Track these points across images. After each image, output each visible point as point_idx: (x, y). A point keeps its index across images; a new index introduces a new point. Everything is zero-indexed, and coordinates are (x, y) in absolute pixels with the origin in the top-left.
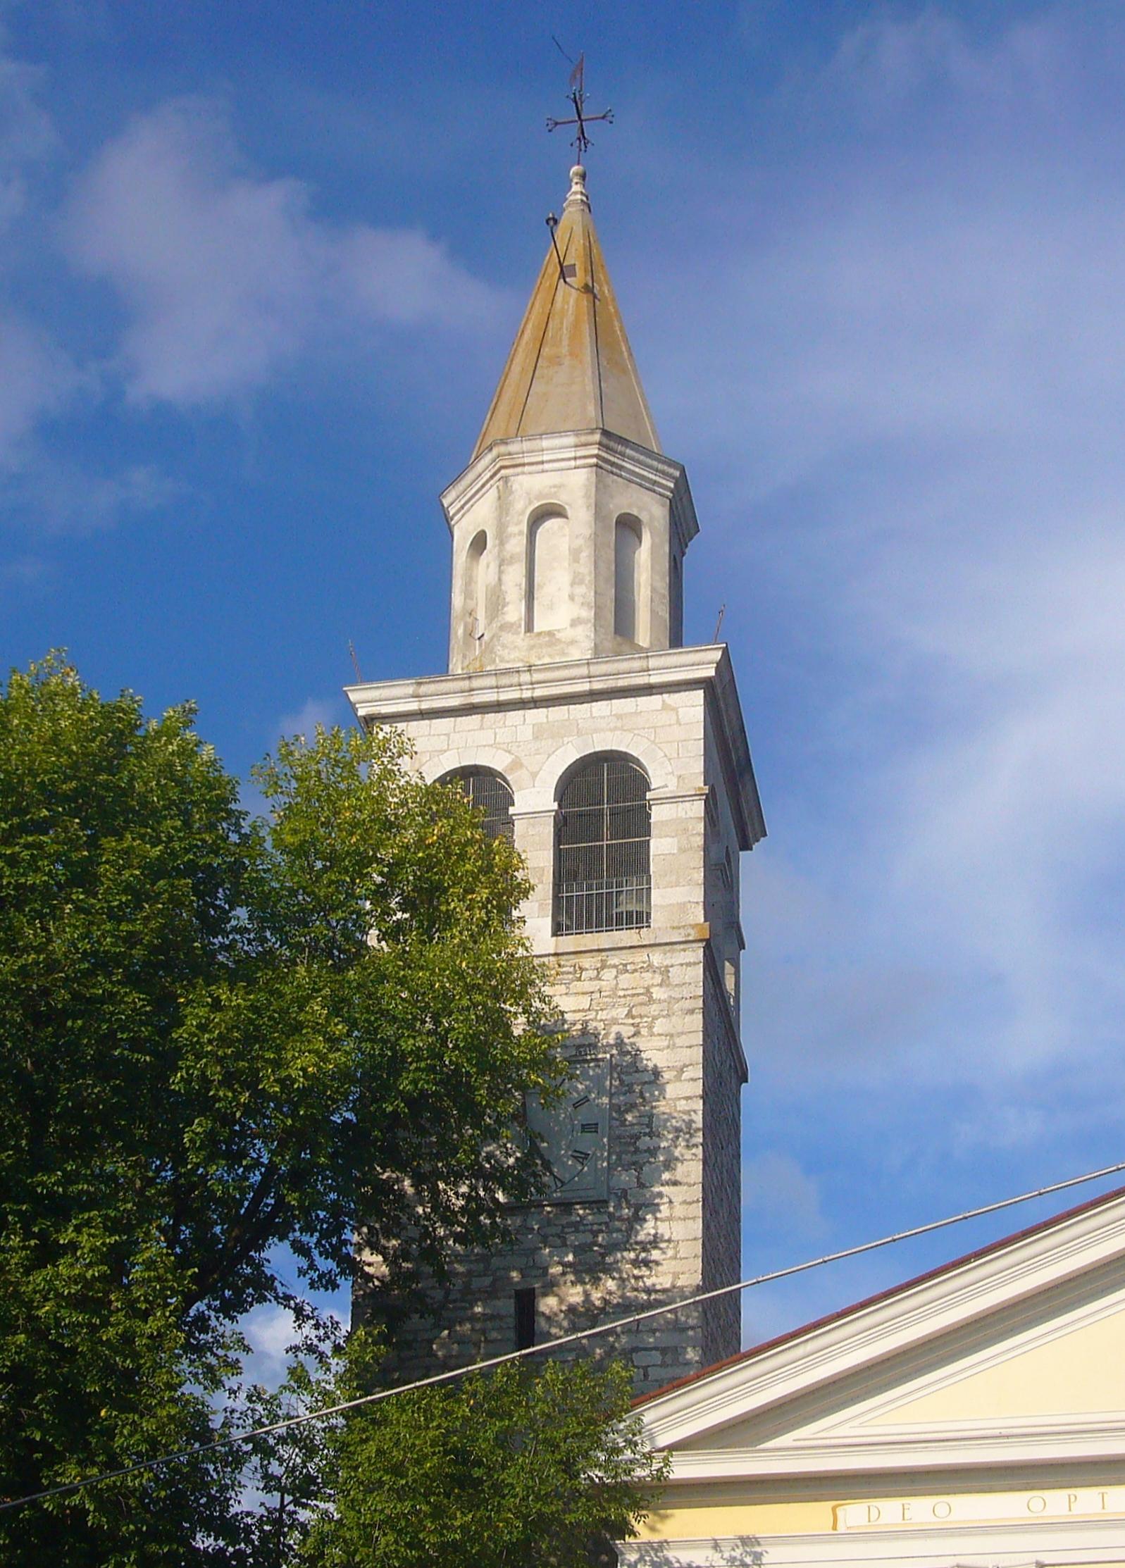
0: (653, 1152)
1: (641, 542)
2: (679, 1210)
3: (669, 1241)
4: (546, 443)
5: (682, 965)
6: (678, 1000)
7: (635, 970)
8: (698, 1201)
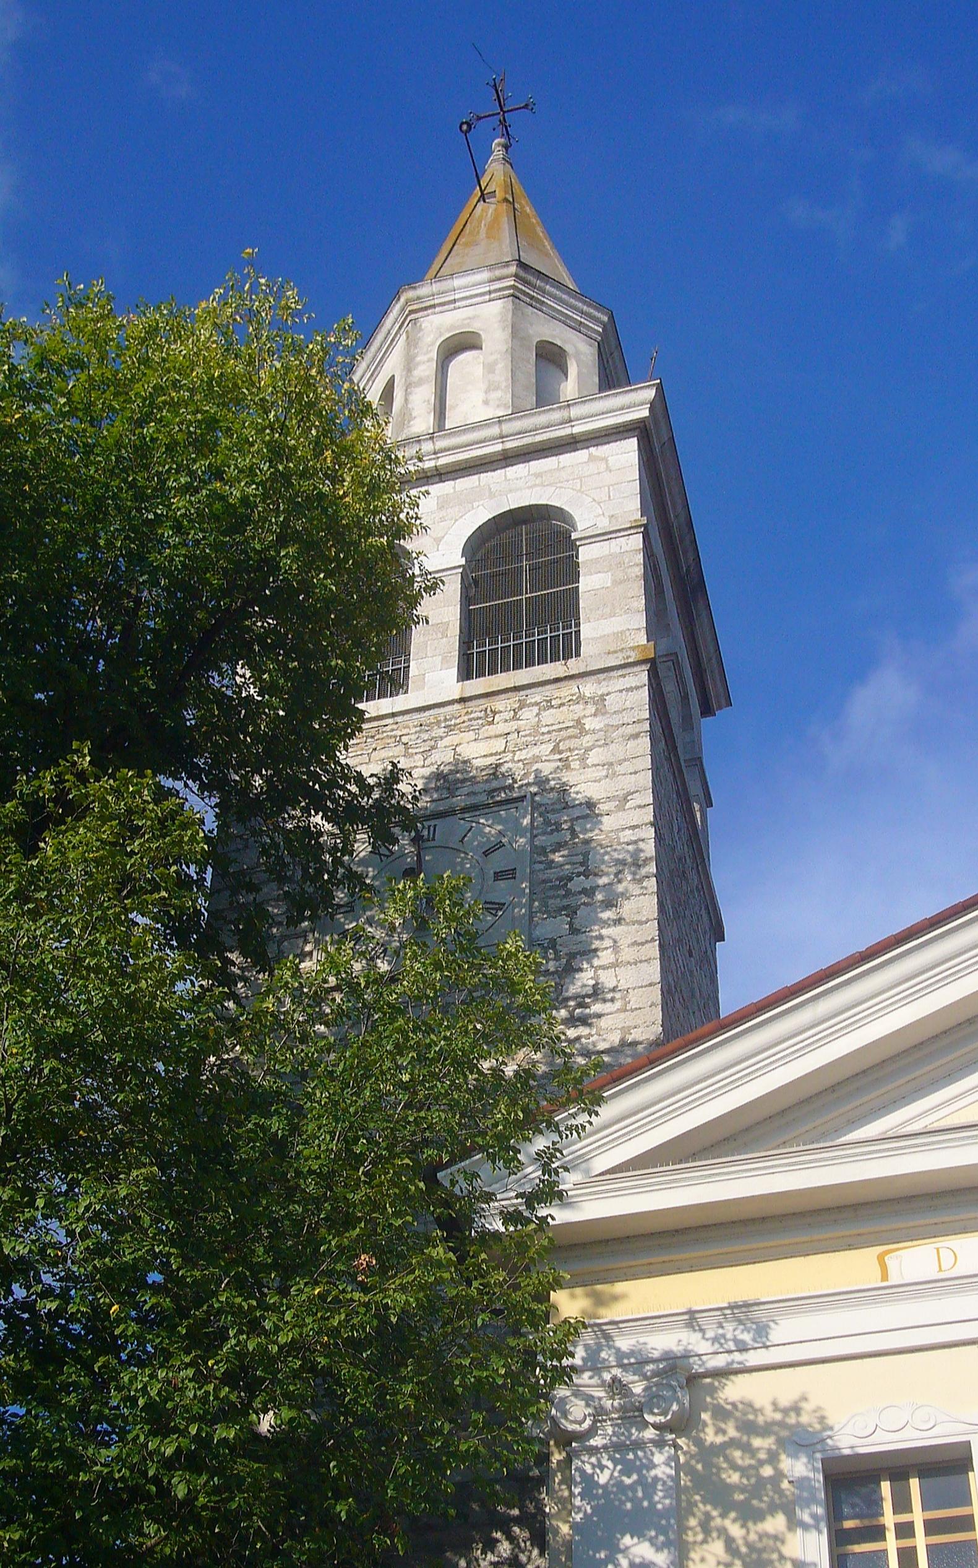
0: (590, 892)
1: (567, 378)
2: (627, 954)
3: (614, 990)
4: (457, 282)
5: (621, 691)
6: (618, 727)
7: (563, 704)
8: (653, 940)
